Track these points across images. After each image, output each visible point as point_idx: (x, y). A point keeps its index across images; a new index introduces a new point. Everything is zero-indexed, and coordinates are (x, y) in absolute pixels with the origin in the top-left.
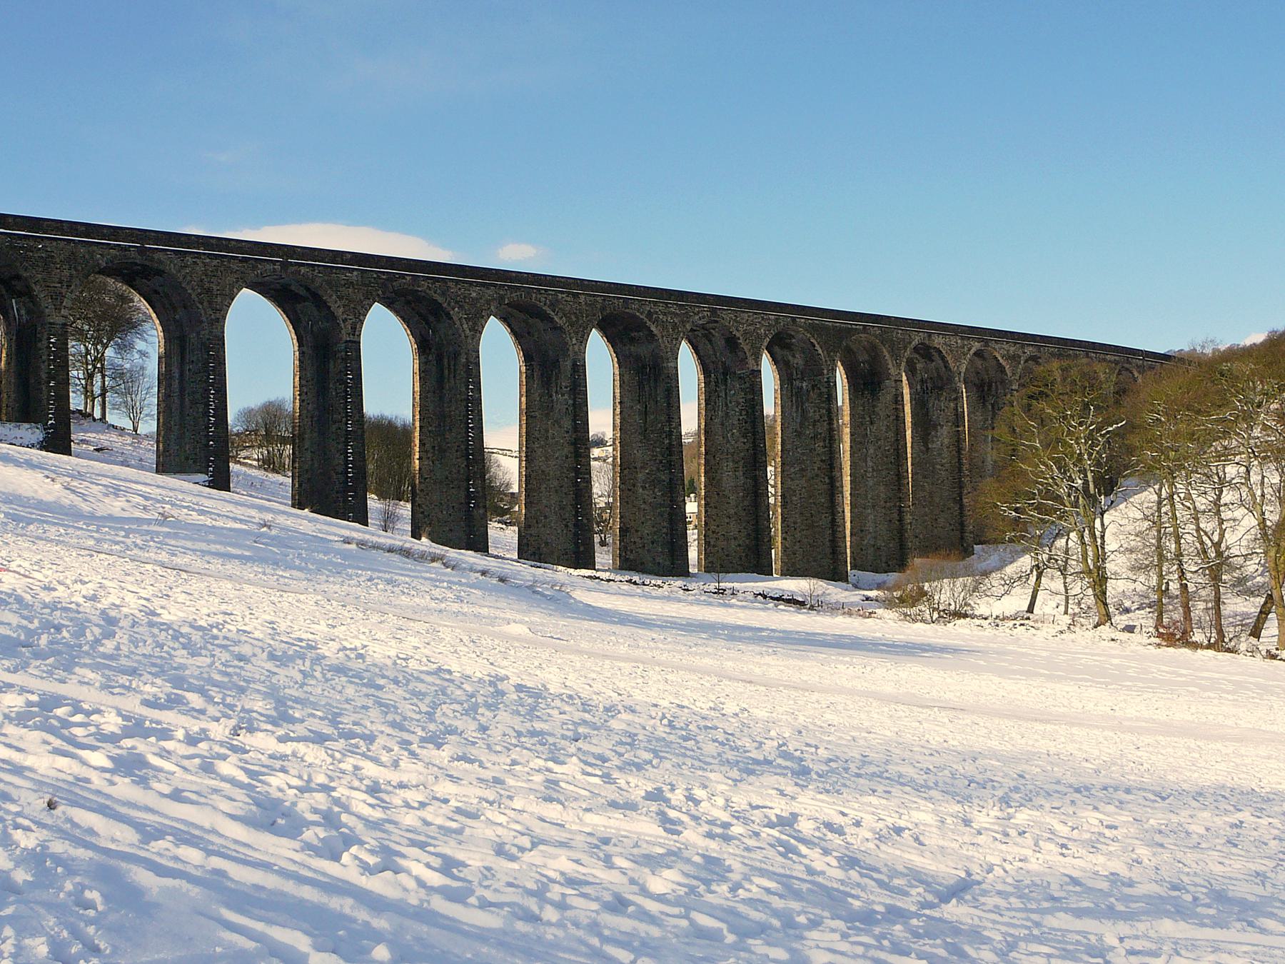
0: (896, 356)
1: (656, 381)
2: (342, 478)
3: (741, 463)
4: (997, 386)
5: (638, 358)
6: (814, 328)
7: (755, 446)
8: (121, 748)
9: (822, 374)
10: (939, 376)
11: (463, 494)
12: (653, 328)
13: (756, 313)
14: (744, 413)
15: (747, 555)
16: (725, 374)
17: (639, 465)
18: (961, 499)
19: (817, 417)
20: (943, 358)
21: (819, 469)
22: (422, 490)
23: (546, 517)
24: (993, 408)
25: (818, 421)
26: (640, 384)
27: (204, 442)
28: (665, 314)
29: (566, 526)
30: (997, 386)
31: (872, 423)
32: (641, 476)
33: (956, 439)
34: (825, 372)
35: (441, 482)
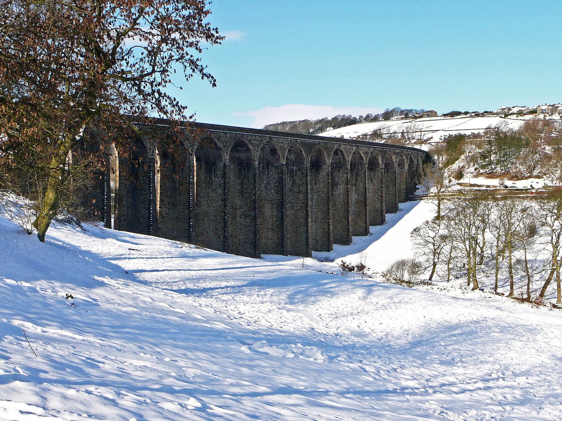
0: (329, 155)
1: (248, 170)
2: (148, 221)
3: (275, 206)
4: (358, 166)
5: (239, 159)
6: (303, 144)
7: (282, 198)
8: (349, 384)
9: (304, 164)
10: (340, 162)
11: (186, 225)
12: (250, 147)
13: (284, 138)
14: (277, 183)
15: (277, 247)
16: (268, 165)
17: (238, 207)
18: (348, 218)
19: (300, 183)
20: (343, 154)
21: (301, 206)
22: (162, 222)
23: (207, 232)
24: (356, 175)
25: (301, 185)
26: (240, 171)
27: (101, 206)
28: (255, 140)
29: (219, 237)
30: (358, 166)
31: (316, 184)
32: (239, 212)
33: (347, 190)
34: (305, 163)
35: (173, 219)
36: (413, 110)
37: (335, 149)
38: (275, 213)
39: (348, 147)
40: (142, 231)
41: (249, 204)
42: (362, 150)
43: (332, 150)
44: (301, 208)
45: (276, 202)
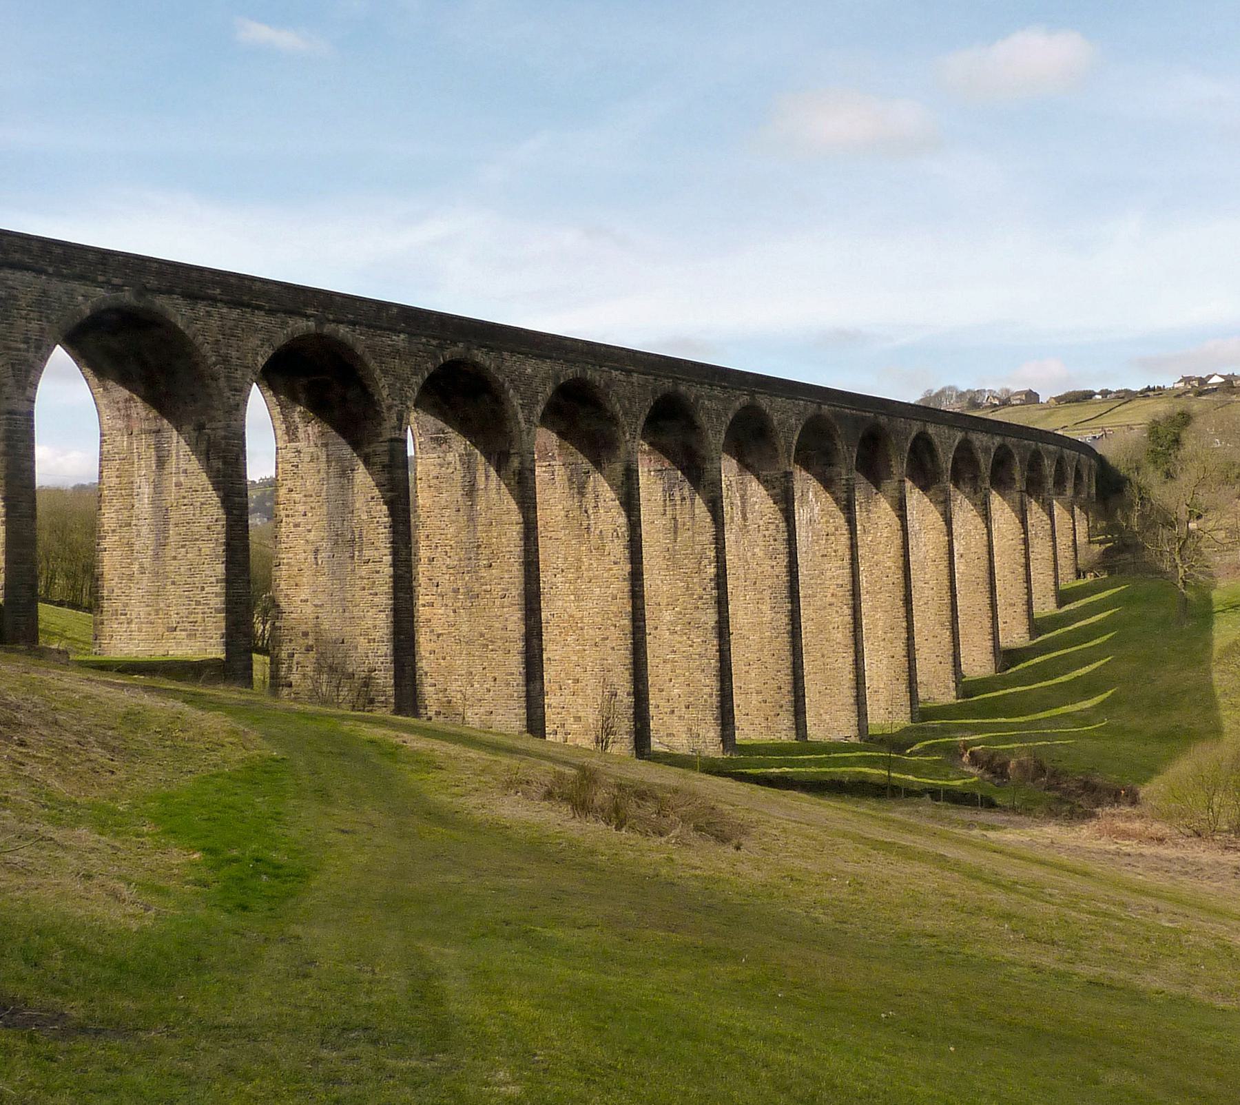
3: (767, 593)
14: (772, 527)
36: (984, 391)
37: (914, 434)
38: (769, 615)
39: (945, 430)
40: (81, 249)
41: (699, 591)
42: (979, 440)
43: (907, 439)
44: (833, 600)
45: (769, 582)
